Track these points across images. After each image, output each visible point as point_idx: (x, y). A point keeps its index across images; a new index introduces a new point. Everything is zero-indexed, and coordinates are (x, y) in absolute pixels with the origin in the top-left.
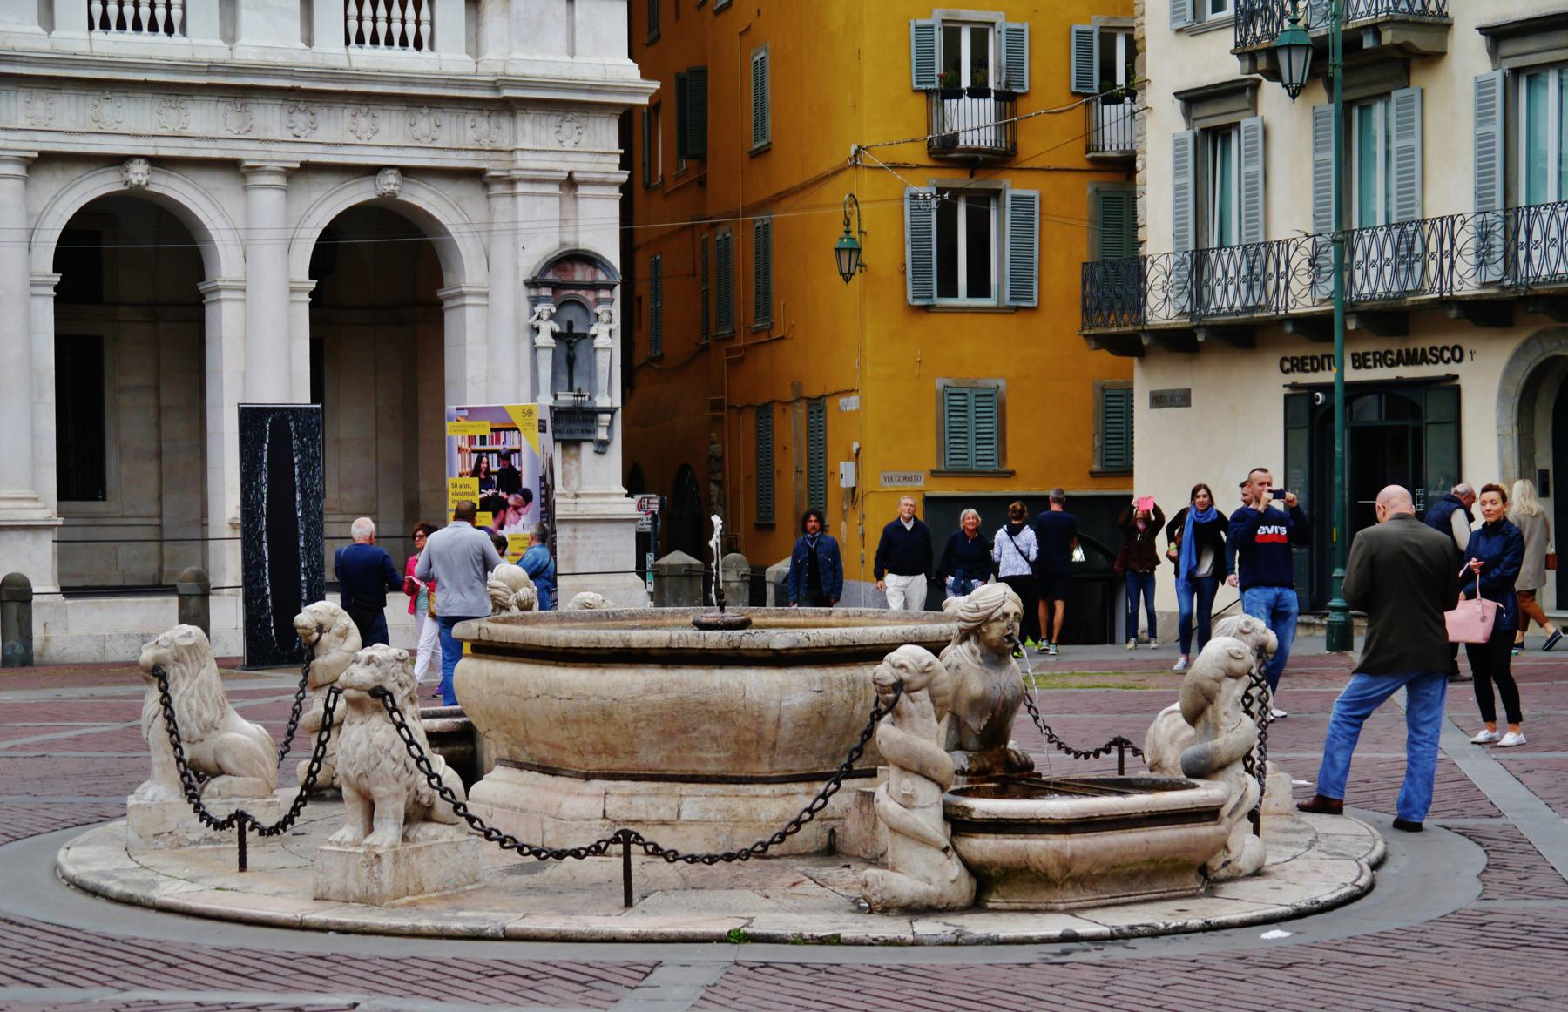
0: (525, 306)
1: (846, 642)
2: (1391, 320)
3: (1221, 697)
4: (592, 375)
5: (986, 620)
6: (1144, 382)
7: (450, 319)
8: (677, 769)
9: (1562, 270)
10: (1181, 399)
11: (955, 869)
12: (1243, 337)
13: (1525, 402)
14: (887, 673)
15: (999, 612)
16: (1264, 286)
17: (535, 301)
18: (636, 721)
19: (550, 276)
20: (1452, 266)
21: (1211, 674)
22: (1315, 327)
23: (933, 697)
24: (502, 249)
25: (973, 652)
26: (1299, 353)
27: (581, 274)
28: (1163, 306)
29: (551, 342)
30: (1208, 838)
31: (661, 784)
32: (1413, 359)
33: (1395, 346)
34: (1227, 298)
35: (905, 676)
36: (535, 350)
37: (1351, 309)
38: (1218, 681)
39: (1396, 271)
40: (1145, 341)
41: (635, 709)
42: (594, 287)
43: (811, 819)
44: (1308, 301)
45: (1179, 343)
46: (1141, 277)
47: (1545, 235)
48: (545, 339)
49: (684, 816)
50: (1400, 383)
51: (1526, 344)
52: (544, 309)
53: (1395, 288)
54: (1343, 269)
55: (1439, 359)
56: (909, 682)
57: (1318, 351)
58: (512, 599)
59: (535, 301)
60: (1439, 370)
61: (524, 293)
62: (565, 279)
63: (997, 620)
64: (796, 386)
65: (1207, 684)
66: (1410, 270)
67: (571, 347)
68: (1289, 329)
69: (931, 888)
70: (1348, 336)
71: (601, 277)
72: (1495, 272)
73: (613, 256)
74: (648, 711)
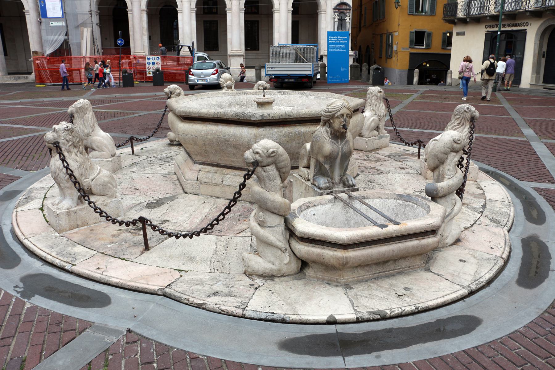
0: (333, 14)
1: (287, 117)
2: (513, 16)
3: (448, 161)
4: (346, 27)
5: (333, 117)
6: (455, 30)
7: (319, 16)
8: (224, 163)
9: (553, 4)
10: (463, 34)
11: (286, 258)
12: (477, 20)
13: (542, 35)
14: (250, 156)
15: (339, 113)
16: (484, 9)
17: (335, 12)
18: (205, 145)
19: (338, 7)
20: (529, 3)
21: (443, 150)
22: (495, 18)
23: (278, 169)
24: (329, 3)
25: (327, 132)
26: (489, 24)
27: (344, 7)
28: (460, 14)
29: (337, 20)
30: (427, 245)
31: (219, 169)
32: (516, 25)
33: (512, 22)
34: (475, 11)
35: (258, 157)
36: (334, 22)
37: (504, 13)
38: (447, 154)
39: (515, 4)
40: (456, 21)
41: (204, 141)
42: (346, 10)
43: (217, 224)
44: (493, 12)
45: (464, 21)
46: (456, 6)
47: (511, 5)
48: (336, 20)
49: (224, 183)
50: (512, 31)
51: (544, 22)
52: (336, 14)
53: (514, 9)
54: (503, 7)
55: (523, 25)
56: (261, 162)
57: (494, 23)
58: (225, 85)
59: (335, 12)
60: (522, 28)
61: (333, 11)
62: (341, 8)
63: (337, 117)
64: (387, 30)
65: (440, 155)
66: (519, 4)
67: (342, 22)
68: (488, 18)
69: (274, 267)
70: (503, 20)
71: (348, 8)
72: (539, 5)
73: (351, 4)
74: (208, 142)
